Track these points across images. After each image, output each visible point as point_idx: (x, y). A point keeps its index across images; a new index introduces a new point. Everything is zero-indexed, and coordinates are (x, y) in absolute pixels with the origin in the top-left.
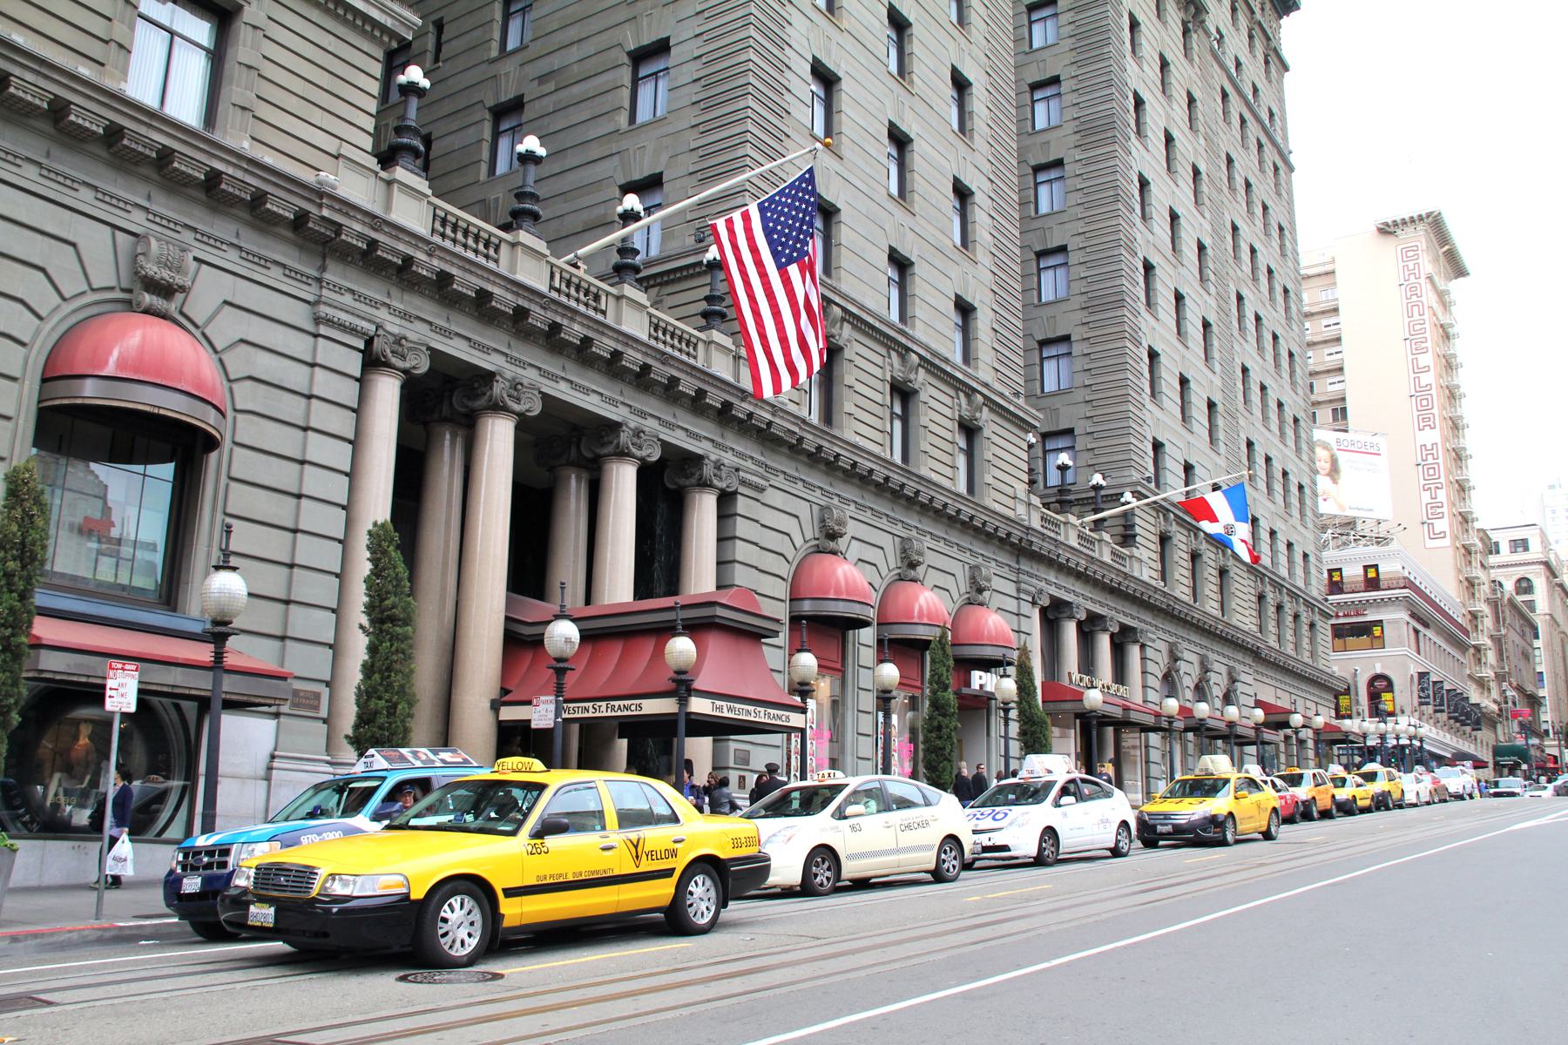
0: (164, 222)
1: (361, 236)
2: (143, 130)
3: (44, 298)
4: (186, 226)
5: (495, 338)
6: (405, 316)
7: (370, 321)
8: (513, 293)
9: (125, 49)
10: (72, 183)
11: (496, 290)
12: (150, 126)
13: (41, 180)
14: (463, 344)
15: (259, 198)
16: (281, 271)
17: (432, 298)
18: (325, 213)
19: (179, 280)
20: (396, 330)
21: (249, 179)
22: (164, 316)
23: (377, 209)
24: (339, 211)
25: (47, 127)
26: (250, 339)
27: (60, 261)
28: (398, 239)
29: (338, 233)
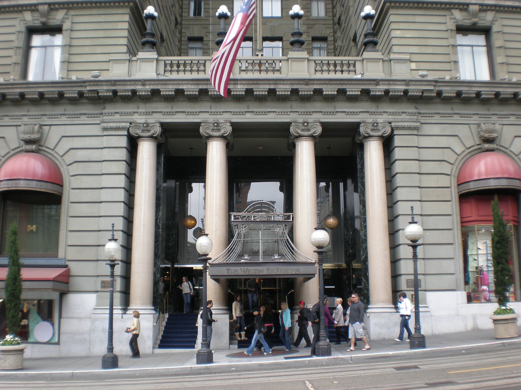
0: (34, 117)
1: (107, 91)
2: (11, 91)
3: (452, 157)
4: (474, 114)
5: (286, 107)
6: (147, 114)
7: (125, 122)
8: (195, 84)
9: (456, 62)
10: (451, 115)
11: (184, 87)
12: (13, 88)
13: (441, 118)
14: (343, 115)
15: (478, 94)
16: (439, 116)
17: (367, 101)
18: (88, 88)
19: (495, 135)
20: (370, 121)
21: (53, 89)
22: (492, 150)
23: (388, 78)
24: (94, 85)
25: (438, 100)
26: (74, 147)
27: (453, 143)
28: (126, 85)
29: (98, 93)
